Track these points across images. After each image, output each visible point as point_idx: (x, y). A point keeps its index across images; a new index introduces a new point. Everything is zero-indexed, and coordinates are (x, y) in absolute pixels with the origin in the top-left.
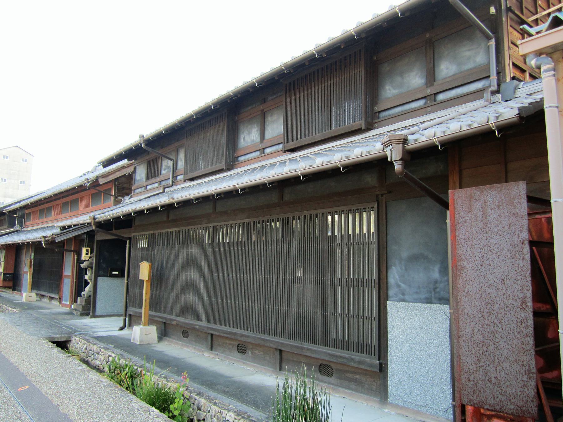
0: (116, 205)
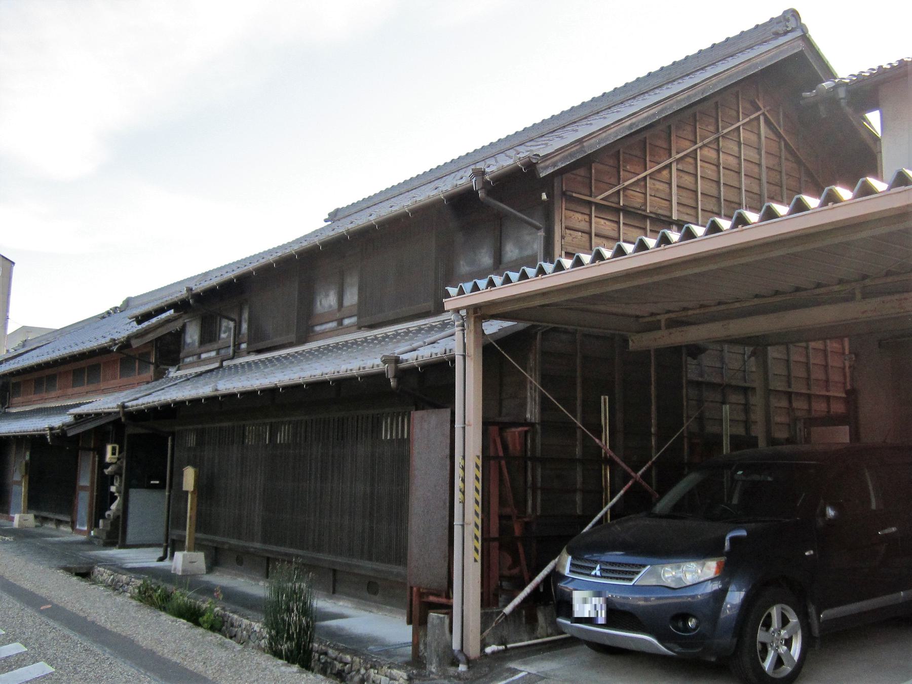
0: (156, 379)
